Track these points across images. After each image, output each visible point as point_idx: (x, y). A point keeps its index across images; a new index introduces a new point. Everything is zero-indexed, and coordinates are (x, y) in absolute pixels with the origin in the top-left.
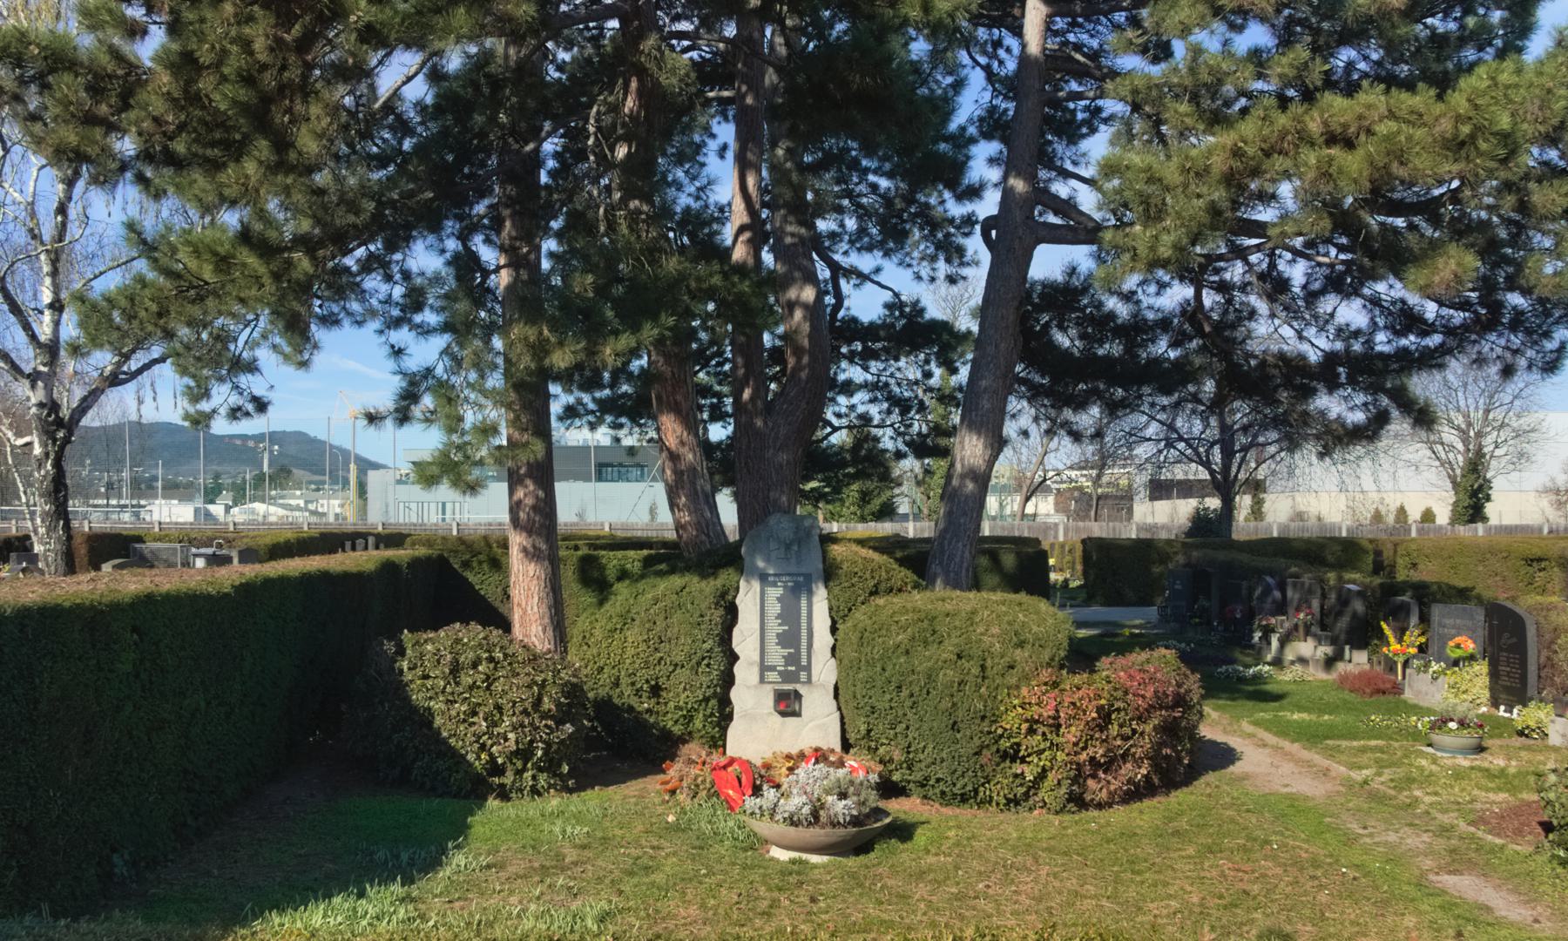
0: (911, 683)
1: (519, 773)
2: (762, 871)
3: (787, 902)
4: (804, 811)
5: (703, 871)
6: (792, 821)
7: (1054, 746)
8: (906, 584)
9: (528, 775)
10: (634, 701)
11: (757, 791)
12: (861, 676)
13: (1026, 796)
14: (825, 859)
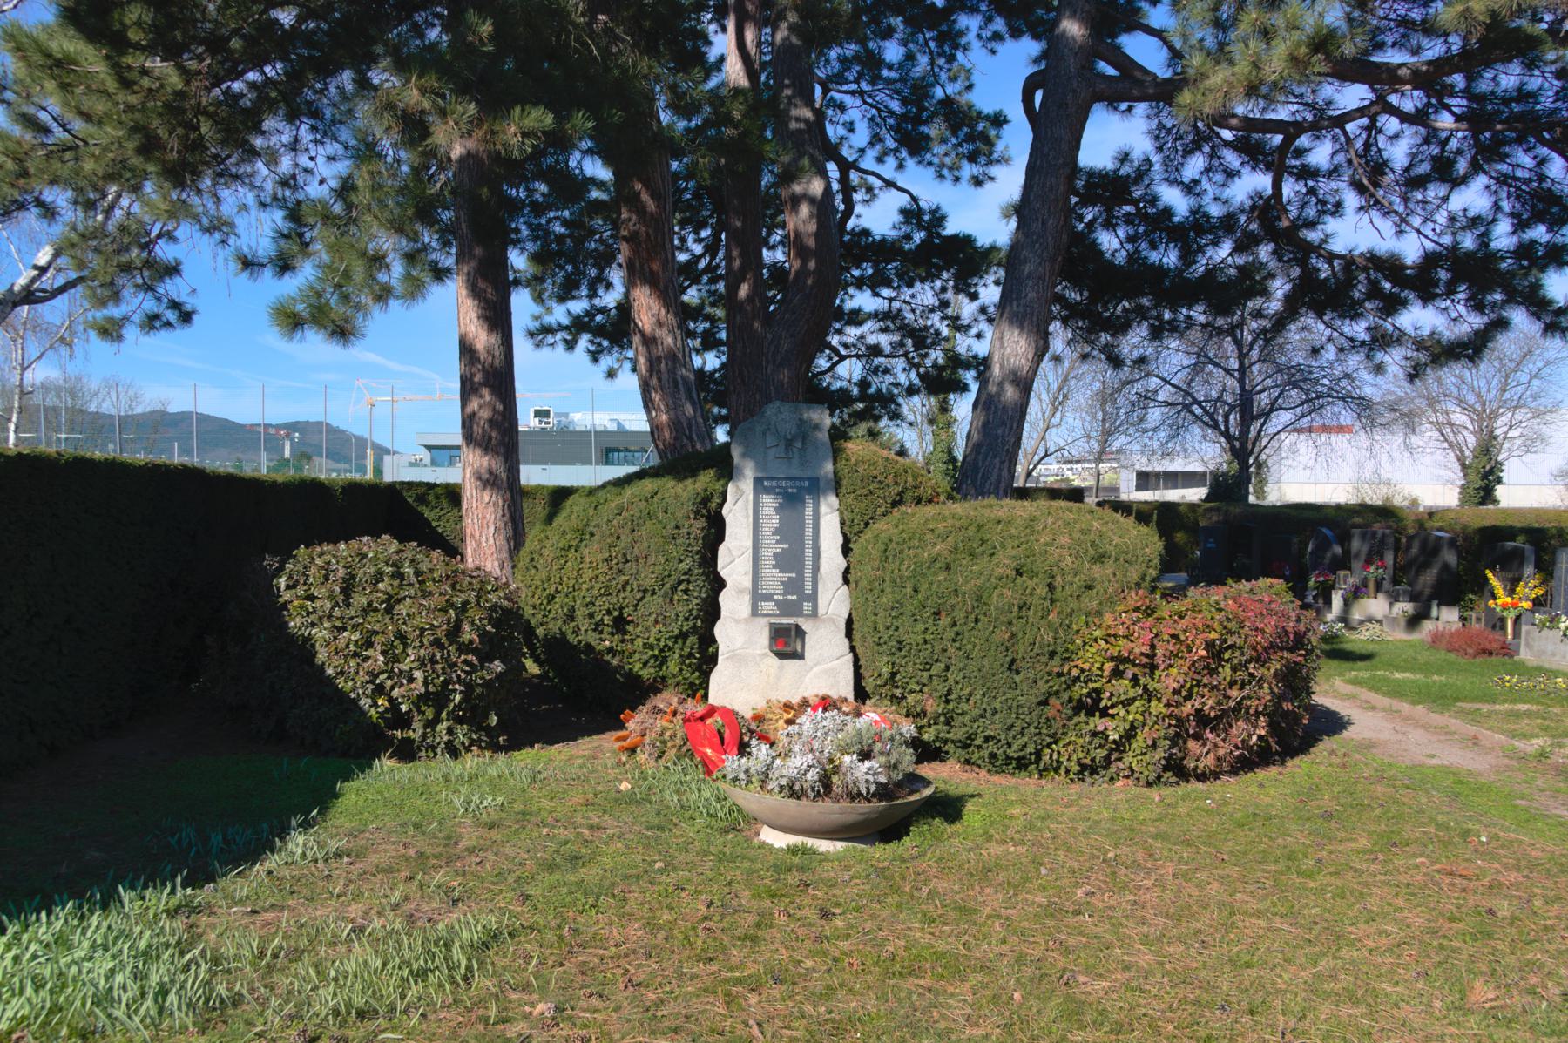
0: (953, 607)
1: (431, 724)
2: (746, 864)
3: (784, 918)
4: (809, 776)
5: (659, 865)
6: (793, 791)
7: (1149, 695)
8: (938, 494)
9: (442, 727)
10: (592, 638)
11: (743, 749)
12: (884, 600)
13: (1108, 761)
14: (840, 846)
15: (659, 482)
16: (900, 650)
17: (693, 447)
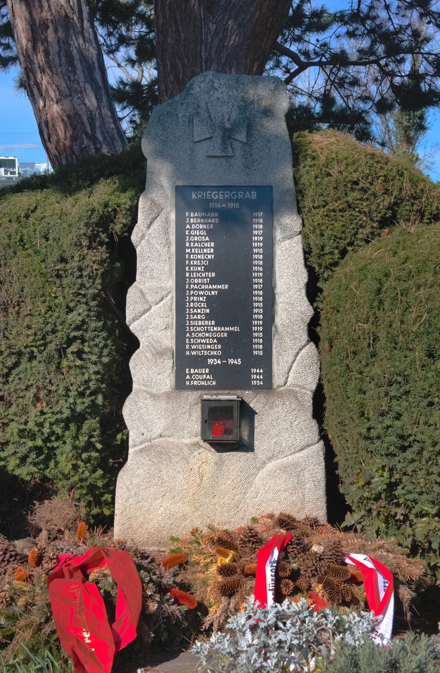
12: (376, 370)
15: (39, 195)
16: (404, 449)
17: (98, 150)
